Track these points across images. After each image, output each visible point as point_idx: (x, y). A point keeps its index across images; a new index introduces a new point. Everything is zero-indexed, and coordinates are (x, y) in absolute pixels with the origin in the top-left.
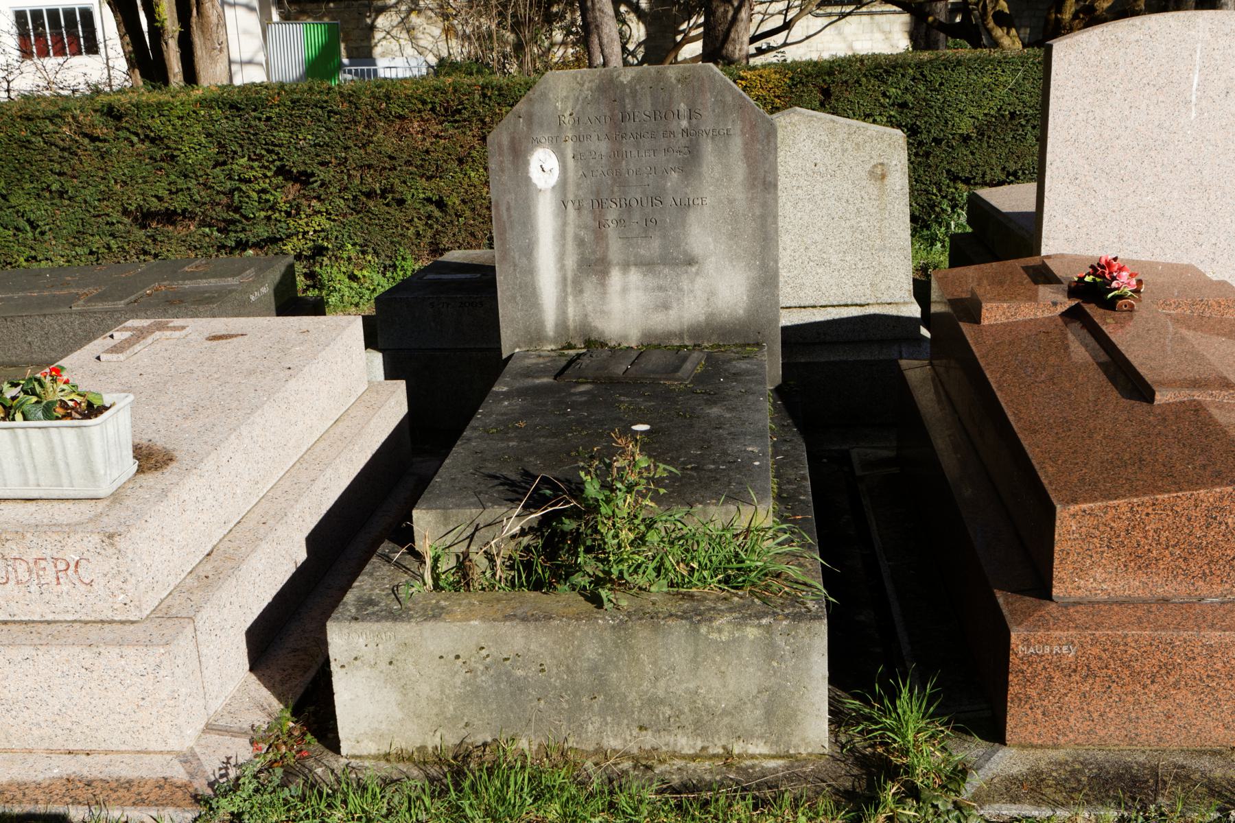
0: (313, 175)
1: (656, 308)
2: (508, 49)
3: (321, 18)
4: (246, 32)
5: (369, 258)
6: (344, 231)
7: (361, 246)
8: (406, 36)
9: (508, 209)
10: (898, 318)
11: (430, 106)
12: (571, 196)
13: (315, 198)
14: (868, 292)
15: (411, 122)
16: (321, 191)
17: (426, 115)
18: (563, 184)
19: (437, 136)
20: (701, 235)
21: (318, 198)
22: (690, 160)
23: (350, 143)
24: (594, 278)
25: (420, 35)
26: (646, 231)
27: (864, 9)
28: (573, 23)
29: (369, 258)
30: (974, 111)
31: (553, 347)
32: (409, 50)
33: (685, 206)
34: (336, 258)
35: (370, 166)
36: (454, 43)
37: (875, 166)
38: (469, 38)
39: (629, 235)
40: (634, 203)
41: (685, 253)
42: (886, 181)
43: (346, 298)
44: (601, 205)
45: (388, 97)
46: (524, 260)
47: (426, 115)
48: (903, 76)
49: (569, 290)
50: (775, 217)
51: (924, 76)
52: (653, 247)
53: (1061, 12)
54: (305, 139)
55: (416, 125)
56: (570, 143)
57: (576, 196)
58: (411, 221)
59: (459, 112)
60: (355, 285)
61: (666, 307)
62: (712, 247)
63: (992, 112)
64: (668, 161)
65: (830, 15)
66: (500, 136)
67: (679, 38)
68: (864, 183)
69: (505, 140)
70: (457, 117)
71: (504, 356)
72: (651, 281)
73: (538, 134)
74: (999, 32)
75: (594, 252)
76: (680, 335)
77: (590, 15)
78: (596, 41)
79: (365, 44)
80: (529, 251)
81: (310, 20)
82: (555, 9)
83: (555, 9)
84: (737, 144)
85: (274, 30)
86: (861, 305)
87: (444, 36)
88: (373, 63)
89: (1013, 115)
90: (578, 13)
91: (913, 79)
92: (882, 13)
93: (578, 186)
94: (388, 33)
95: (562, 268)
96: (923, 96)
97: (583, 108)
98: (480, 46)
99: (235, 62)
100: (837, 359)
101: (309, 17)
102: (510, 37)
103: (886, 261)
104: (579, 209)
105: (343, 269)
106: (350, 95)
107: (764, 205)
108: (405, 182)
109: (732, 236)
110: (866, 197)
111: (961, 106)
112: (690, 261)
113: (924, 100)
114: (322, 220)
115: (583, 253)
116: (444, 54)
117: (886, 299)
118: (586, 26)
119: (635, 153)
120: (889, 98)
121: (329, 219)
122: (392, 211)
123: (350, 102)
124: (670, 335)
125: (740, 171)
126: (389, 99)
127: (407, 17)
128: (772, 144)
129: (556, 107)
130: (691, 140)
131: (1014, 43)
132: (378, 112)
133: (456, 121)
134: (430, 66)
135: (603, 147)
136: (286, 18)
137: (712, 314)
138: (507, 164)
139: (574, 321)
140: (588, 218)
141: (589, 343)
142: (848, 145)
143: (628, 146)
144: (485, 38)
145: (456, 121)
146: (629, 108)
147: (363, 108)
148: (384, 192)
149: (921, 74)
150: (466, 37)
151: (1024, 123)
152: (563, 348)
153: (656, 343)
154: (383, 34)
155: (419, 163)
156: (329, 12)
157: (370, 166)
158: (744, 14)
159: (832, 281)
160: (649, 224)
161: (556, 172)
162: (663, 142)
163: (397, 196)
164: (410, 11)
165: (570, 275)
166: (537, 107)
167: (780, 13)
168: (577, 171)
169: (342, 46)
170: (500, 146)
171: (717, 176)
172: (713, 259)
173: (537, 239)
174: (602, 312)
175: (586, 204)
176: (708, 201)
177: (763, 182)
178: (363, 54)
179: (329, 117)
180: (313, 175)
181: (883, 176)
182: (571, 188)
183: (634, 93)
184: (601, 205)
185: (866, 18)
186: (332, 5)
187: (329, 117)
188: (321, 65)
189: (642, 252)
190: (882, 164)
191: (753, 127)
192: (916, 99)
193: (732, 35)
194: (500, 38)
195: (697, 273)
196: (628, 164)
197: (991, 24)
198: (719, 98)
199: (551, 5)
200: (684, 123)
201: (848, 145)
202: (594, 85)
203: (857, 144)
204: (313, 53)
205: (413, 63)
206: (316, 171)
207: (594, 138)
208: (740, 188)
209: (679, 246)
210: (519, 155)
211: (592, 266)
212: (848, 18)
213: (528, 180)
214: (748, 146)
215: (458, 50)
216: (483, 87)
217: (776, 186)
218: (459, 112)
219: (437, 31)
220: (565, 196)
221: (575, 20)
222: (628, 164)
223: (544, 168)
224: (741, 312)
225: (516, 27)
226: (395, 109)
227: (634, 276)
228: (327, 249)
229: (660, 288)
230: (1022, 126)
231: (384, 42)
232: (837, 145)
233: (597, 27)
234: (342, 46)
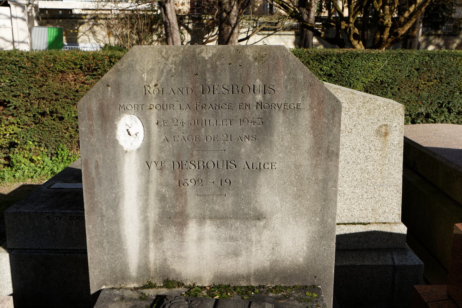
0: (9, 102)
1: (228, 255)
2: (134, 42)
3: (56, 26)
4: (21, 29)
5: (42, 149)
6: (27, 134)
7: (38, 142)
8: (92, 35)
9: (97, 167)
10: (391, 234)
11: (79, 66)
12: (154, 158)
13: (11, 115)
14: (370, 215)
15: (68, 74)
16: (15, 111)
17: (77, 71)
18: (147, 147)
19: (83, 83)
20: (269, 195)
21: (12, 115)
22: (262, 130)
23: (32, 85)
24: (173, 229)
25: (97, 35)
26: (220, 190)
27: (277, 33)
28: (161, 33)
29: (42, 149)
30: (364, 79)
31: (136, 285)
32: (93, 41)
33: (257, 169)
34: (23, 149)
35: (43, 98)
36: (112, 39)
37: (381, 127)
38: (118, 37)
39: (206, 193)
40: (211, 165)
41: (255, 209)
42: (388, 138)
43: (26, 173)
44: (181, 166)
45: (55, 60)
46: (111, 212)
47: (77, 71)
48: (331, 60)
49: (151, 238)
50: (336, 181)
51: (341, 61)
52: (227, 203)
53: (383, 35)
54: (5, 82)
55: (71, 76)
56: (154, 111)
57: (159, 158)
58: (67, 129)
59: (96, 70)
60: (33, 165)
61: (236, 254)
62: (278, 205)
63: (372, 80)
64: (243, 130)
65: (264, 34)
66: (89, 103)
67: (204, 41)
68: (372, 138)
69: (95, 106)
70: (95, 73)
71: (92, 292)
72: (224, 232)
73: (124, 101)
74: (355, 42)
75: (174, 207)
76: (248, 278)
77: (168, 29)
78: (171, 40)
79: (74, 37)
80: (115, 204)
81: (51, 26)
82: (154, 27)
83: (154, 27)
84: (305, 117)
85: (35, 30)
86: (364, 224)
87: (108, 36)
88: (77, 45)
89: (382, 82)
90: (164, 29)
91: (335, 62)
92: (284, 35)
93: (161, 149)
94: (84, 33)
95: (145, 219)
96: (340, 71)
97: (167, 79)
98: (122, 40)
99: (16, 42)
100: (348, 263)
101: (51, 25)
102: (136, 37)
103: (384, 194)
104: (161, 169)
105: (26, 156)
106: (32, 58)
107: (327, 171)
108: (64, 108)
109: (298, 196)
110: (373, 148)
111: (358, 77)
112: (259, 217)
113: (340, 73)
114: (15, 128)
115: (163, 208)
116: (108, 43)
117: (382, 220)
118: (167, 35)
119: (213, 122)
120: (323, 71)
121: (19, 127)
122: (56, 124)
123: (32, 62)
124: (239, 277)
125: (307, 141)
126: (55, 61)
127: (92, 27)
128: (336, 119)
129: (142, 78)
130: (264, 112)
131: (361, 48)
132: (49, 69)
133: (94, 75)
134: (101, 47)
135: (185, 115)
136: (41, 25)
137: (276, 261)
138: (96, 127)
139: (155, 264)
140: (170, 179)
141: (168, 283)
142: (363, 111)
143: (207, 115)
144: (124, 37)
145: (94, 75)
146: (209, 81)
147: (40, 66)
148: (52, 113)
149: (340, 60)
150: (116, 36)
151: (387, 86)
152: (144, 287)
153: (226, 283)
154: (82, 33)
155: (72, 97)
156: (59, 23)
157: (43, 98)
158: (236, 31)
159: (345, 207)
160: (224, 184)
161: (141, 135)
162: (240, 114)
163: (59, 115)
164: (94, 24)
165: (152, 226)
166: (124, 77)
167: (245, 33)
168: (160, 136)
169: (64, 38)
170: (89, 111)
171: (286, 144)
172: (279, 215)
173: (123, 194)
174: (180, 257)
175: (168, 165)
176: (277, 166)
177: (326, 150)
178: (73, 41)
179: (20, 70)
180: (9, 102)
181: (386, 134)
182: (155, 151)
183: (214, 69)
184: (181, 166)
185: (278, 36)
186: (60, 20)
187: (20, 70)
188: (55, 44)
189: (217, 207)
190: (386, 125)
191: (321, 102)
192: (336, 72)
193: (231, 39)
194: (131, 37)
195: (264, 227)
196: (206, 131)
197: (352, 39)
198: (292, 76)
199: (152, 25)
200: (259, 97)
201: (363, 111)
202: (177, 59)
203: (369, 110)
204: (51, 39)
205: (94, 46)
206: (11, 100)
207: (177, 107)
208: (306, 155)
209: (250, 203)
210: (107, 120)
211: (172, 217)
212: (271, 36)
213: (115, 142)
214: (315, 119)
215: (113, 41)
216: (110, 57)
217: (337, 155)
218: (96, 70)
219: (105, 33)
220: (149, 157)
221: (162, 31)
222: (206, 131)
223: (130, 131)
224: (301, 259)
225: (138, 33)
226: (59, 67)
227: (209, 228)
228: (17, 144)
229: (232, 239)
230: (386, 87)
231: (82, 37)
232: (354, 110)
233: (171, 34)
234: (64, 38)
